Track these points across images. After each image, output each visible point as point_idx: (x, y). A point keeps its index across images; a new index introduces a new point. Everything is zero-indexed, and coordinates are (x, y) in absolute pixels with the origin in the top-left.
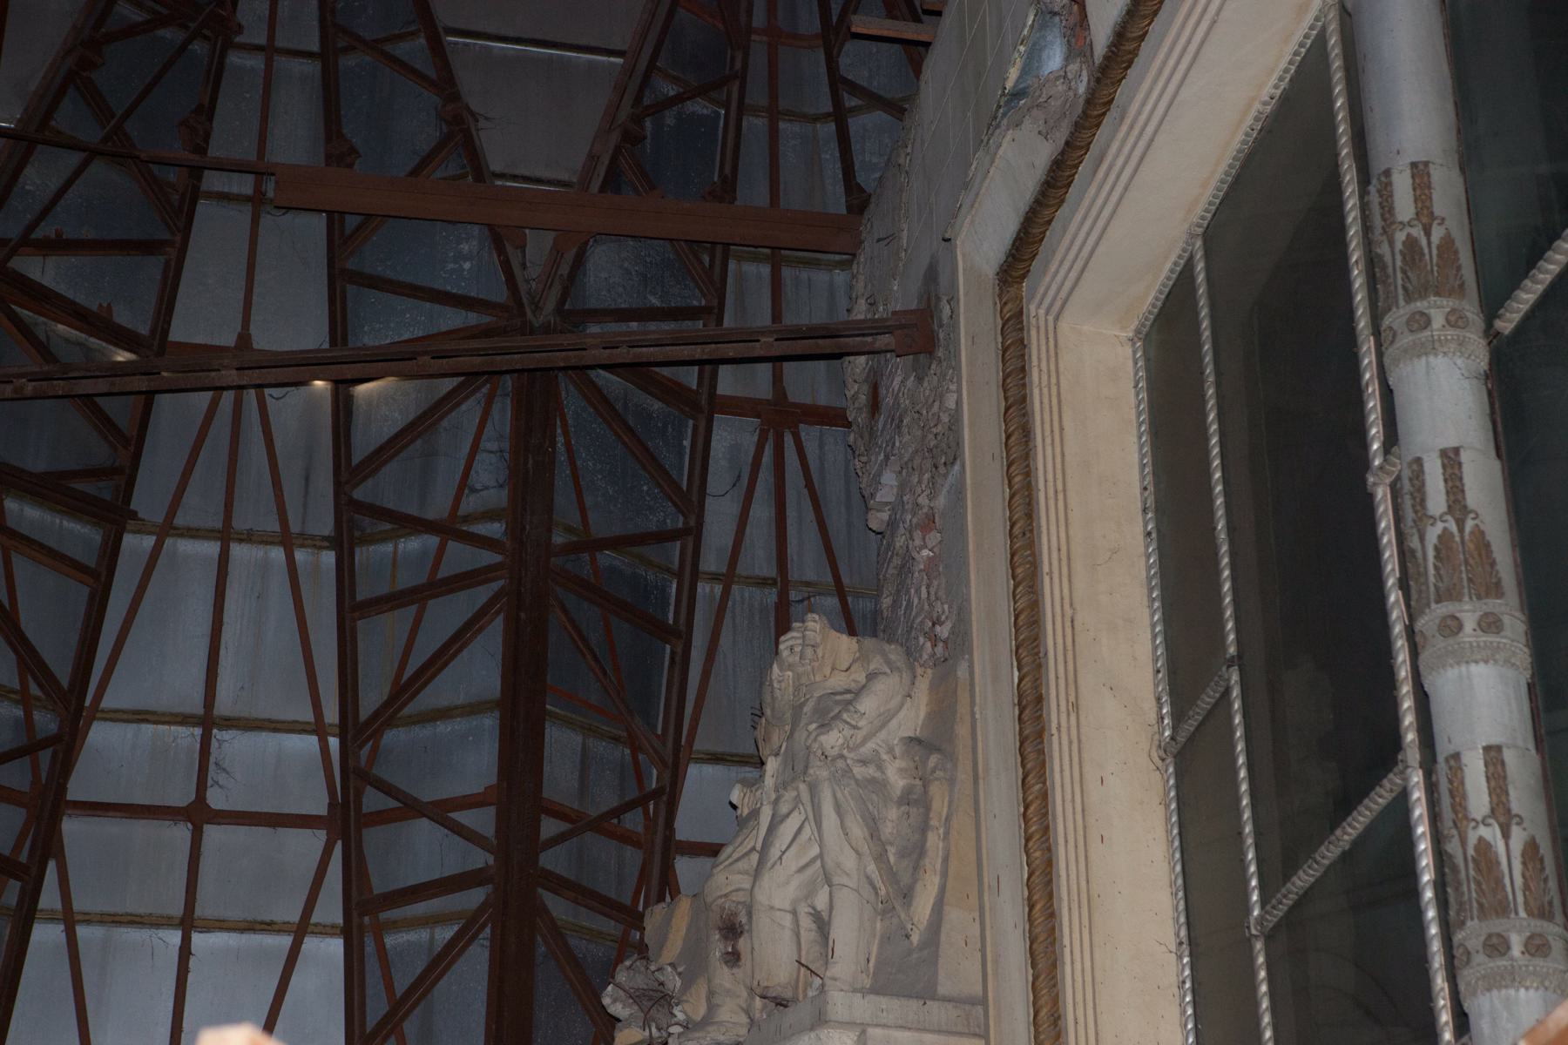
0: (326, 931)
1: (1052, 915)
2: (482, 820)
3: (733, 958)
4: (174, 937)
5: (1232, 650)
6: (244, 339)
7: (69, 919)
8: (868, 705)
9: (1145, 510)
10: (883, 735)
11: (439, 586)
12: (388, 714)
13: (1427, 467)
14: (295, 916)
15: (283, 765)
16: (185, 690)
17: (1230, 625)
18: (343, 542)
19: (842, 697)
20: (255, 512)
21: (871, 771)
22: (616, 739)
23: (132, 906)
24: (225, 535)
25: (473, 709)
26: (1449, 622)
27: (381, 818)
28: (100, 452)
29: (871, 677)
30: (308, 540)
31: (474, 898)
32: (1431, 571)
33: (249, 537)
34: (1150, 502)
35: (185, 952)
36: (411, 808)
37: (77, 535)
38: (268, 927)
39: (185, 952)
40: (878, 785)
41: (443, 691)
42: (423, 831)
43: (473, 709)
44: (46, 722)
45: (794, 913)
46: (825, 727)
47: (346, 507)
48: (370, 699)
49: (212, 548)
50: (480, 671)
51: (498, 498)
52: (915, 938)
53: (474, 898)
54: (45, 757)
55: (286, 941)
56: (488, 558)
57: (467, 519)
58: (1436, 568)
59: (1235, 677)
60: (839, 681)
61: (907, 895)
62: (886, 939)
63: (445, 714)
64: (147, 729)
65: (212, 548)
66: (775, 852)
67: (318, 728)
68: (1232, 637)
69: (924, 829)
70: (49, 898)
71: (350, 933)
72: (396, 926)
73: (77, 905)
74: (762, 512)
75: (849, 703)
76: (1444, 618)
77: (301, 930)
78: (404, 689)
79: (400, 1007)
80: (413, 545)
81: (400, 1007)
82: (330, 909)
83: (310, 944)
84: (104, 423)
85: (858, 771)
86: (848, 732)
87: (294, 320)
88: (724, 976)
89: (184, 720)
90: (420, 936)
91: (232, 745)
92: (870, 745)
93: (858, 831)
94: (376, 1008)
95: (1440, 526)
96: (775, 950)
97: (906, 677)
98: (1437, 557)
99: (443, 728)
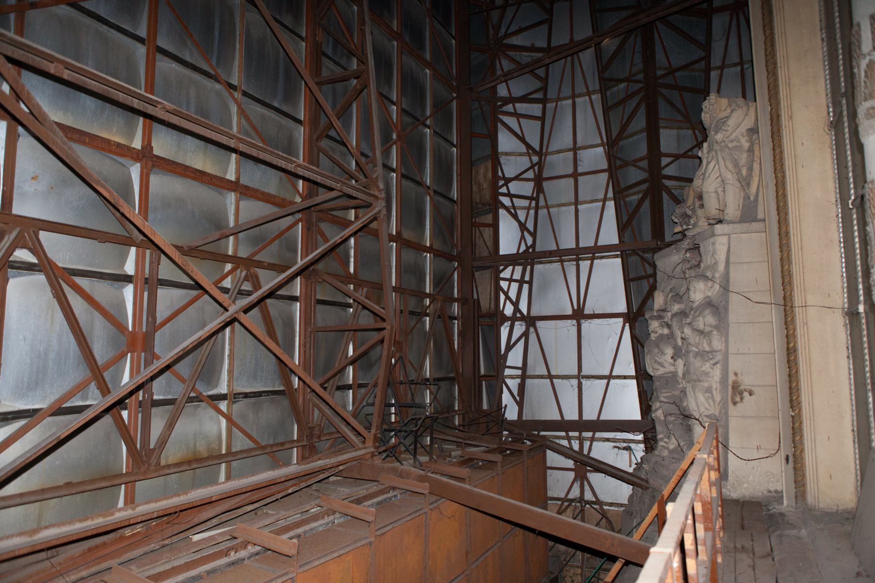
0: (610, 199)
1: (785, 196)
2: (644, 164)
3: (702, 206)
4: (573, 207)
5: (843, 90)
6: (572, 40)
7: (547, 207)
8: (731, 122)
9: (821, 30)
10: (739, 130)
11: (629, 97)
12: (620, 137)
13: (863, 27)
14: (602, 197)
15: (595, 157)
16: (568, 141)
17: (842, 79)
18: (603, 91)
19: (729, 119)
20: (580, 88)
21: (735, 143)
22: (688, 128)
23: (563, 201)
24: (573, 97)
25: (641, 131)
26: (871, 111)
27: (621, 167)
28: (538, 84)
29: (732, 111)
30: (594, 92)
31: (644, 187)
32: (863, 84)
33: (580, 96)
34: (823, 26)
35: (577, 211)
36: (627, 164)
37: (535, 109)
38: (597, 201)
39: (577, 211)
40: (739, 148)
41: (632, 128)
42: (632, 170)
43: (641, 131)
44: (535, 159)
45: (717, 192)
46: (717, 132)
47: (602, 79)
48: (614, 134)
49: (570, 101)
50: (640, 122)
51: (641, 66)
52: (752, 198)
53: (644, 187)
54: (536, 168)
55: (601, 203)
56: (641, 85)
57: (634, 75)
58: (865, 82)
59: (844, 101)
60: (722, 115)
61: (748, 185)
62: (745, 198)
63: (631, 136)
64: (561, 154)
65: (570, 101)
66: (707, 175)
67: (602, 145)
68: (843, 84)
69: (753, 161)
70: (542, 203)
71: (615, 199)
72: (627, 196)
73: (549, 204)
74: (733, 41)
75: (725, 122)
76: (868, 109)
77: (605, 200)
78: (624, 128)
79: (632, 216)
80: (622, 85)
81: (632, 216)
82: (610, 194)
83: (607, 203)
84: (538, 77)
85: (730, 145)
86: (724, 132)
87: (584, 31)
88: (700, 212)
89: (569, 150)
90: (636, 197)
91: (582, 154)
92: (734, 135)
93: (730, 166)
94: (625, 218)
95: (868, 58)
96: (712, 205)
97: (745, 109)
98: (866, 76)
99: (635, 138)
